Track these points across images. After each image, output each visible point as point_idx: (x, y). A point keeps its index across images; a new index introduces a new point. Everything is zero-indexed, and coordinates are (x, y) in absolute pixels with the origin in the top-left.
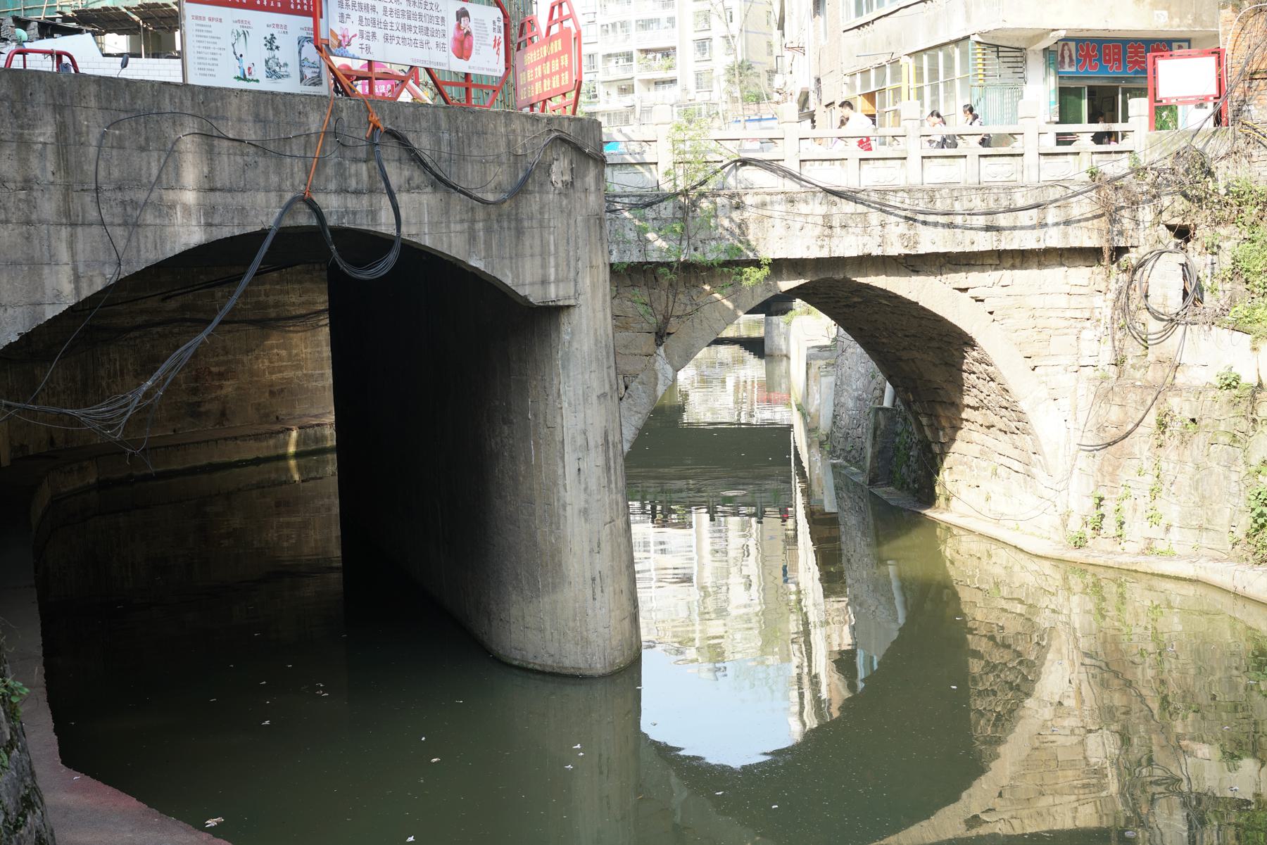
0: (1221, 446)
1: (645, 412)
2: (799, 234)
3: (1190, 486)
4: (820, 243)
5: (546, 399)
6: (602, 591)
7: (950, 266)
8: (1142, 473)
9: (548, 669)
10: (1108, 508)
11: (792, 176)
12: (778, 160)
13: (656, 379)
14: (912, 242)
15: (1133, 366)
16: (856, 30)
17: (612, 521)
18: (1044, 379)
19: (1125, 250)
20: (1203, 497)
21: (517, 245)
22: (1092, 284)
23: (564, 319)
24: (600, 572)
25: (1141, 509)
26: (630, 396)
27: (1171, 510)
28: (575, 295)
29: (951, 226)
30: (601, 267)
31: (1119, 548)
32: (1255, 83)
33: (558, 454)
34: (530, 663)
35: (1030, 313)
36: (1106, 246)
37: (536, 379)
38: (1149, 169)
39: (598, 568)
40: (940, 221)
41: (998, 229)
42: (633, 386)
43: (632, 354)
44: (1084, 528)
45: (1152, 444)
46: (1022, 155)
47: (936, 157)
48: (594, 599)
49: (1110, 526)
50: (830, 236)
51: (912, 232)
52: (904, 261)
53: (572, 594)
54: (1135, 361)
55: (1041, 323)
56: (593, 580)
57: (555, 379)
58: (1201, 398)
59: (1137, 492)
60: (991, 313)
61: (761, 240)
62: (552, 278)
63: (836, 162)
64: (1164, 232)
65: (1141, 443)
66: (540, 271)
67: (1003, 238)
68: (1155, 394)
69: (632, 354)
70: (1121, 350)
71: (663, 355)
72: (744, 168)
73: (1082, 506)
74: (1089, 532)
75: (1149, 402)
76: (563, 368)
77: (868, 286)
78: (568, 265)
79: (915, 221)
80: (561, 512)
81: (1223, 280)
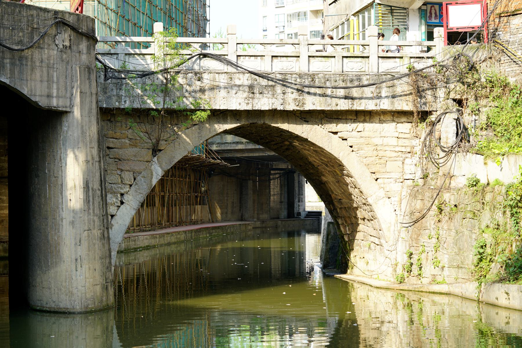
0: (468, 219)
1: (145, 193)
2: (234, 96)
3: (453, 243)
4: (246, 102)
5: (55, 162)
6: (81, 267)
7: (327, 119)
8: (430, 238)
9: (52, 310)
10: (415, 259)
11: (229, 63)
12: (224, 55)
13: (152, 175)
14: (301, 103)
15: (432, 179)
16: (334, 4)
17: (89, 230)
18: (382, 186)
19: (429, 113)
20: (460, 249)
21: (31, 74)
22: (412, 132)
23: (64, 119)
24: (80, 256)
25: (430, 258)
26: (136, 184)
27: (444, 258)
28: (70, 106)
29: (324, 95)
30: (88, 94)
31: (419, 282)
32: (502, 19)
33: (59, 191)
34: (44, 307)
35: (374, 148)
36: (415, 110)
37: (50, 152)
38: (438, 65)
39: (79, 254)
40: (318, 92)
41: (353, 99)
42: (138, 178)
43: (138, 161)
44: (404, 272)
45: (436, 221)
46: (368, 57)
47: (317, 57)
48: (76, 270)
49: (415, 270)
50: (253, 98)
51: (301, 98)
52: (299, 115)
53: (65, 268)
54: (433, 176)
55: (381, 153)
56: (76, 260)
57: (59, 151)
58: (459, 193)
59: (429, 249)
60: (351, 147)
61: (212, 99)
62: (55, 95)
63: (258, 58)
64: (451, 102)
65: (430, 221)
66: (46, 90)
67: (355, 103)
68: (438, 192)
69: (138, 161)
70: (426, 170)
71: (157, 162)
72: (204, 59)
73: (403, 259)
74: (406, 274)
75: (435, 197)
76: (63, 145)
77: (278, 128)
78: (66, 89)
79: (303, 91)
80: (60, 223)
81: (482, 129)
